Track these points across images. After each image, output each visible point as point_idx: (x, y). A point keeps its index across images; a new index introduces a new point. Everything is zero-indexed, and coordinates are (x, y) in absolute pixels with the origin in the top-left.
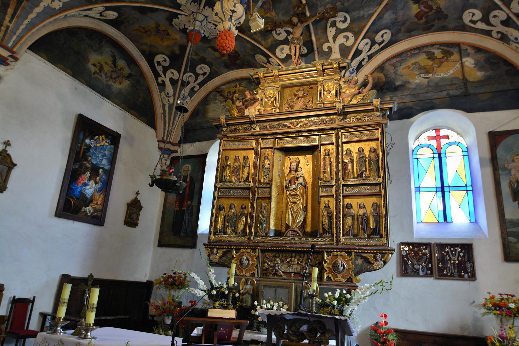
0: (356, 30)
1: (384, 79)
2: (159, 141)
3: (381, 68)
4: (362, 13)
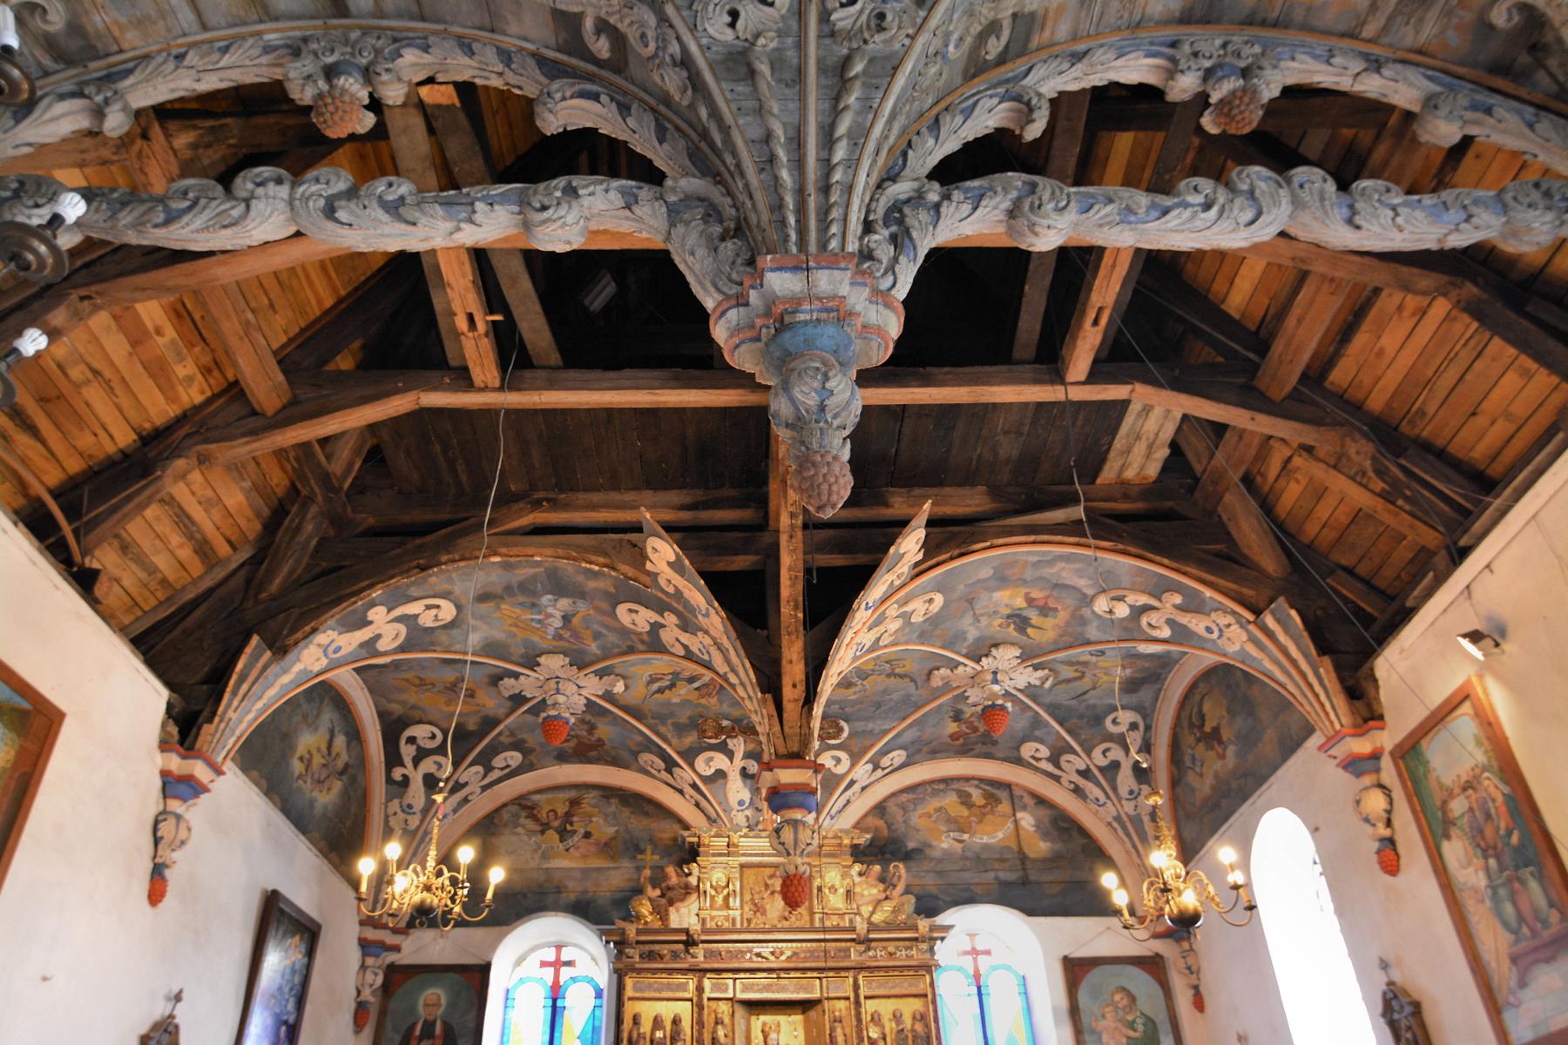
0: (856, 750)
1: (885, 832)
2: (362, 923)
3: (880, 809)
4: (870, 726)
